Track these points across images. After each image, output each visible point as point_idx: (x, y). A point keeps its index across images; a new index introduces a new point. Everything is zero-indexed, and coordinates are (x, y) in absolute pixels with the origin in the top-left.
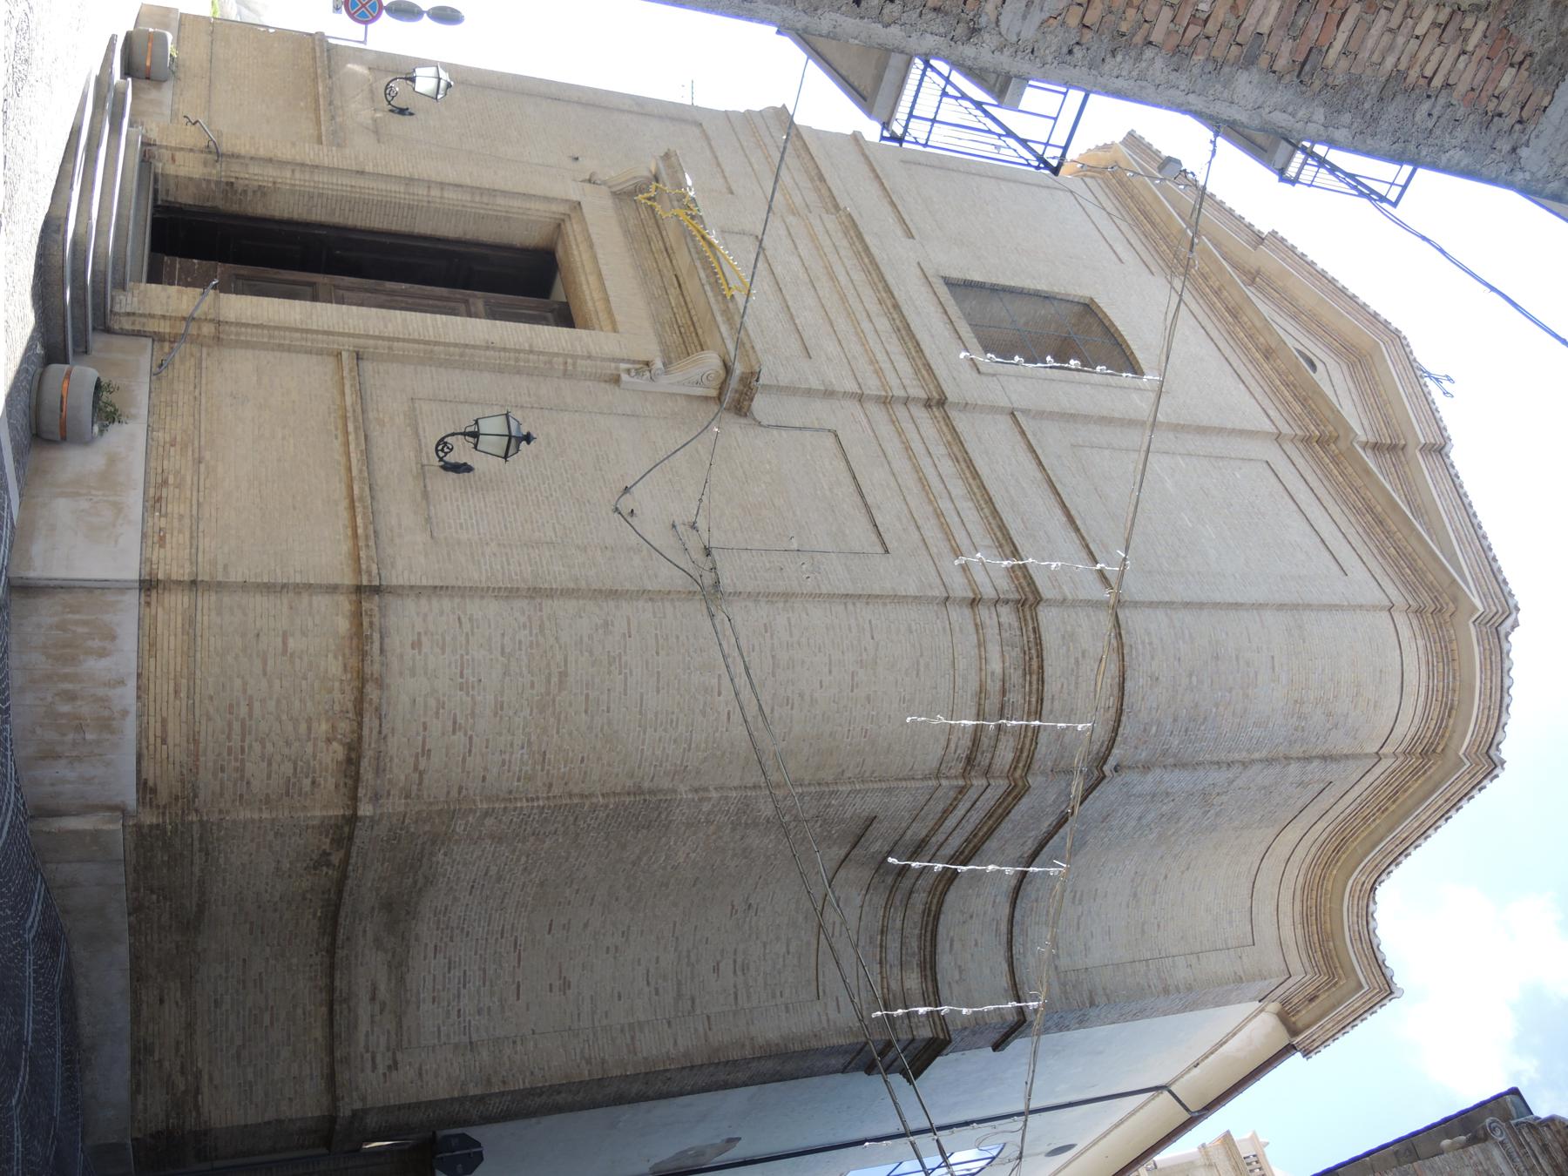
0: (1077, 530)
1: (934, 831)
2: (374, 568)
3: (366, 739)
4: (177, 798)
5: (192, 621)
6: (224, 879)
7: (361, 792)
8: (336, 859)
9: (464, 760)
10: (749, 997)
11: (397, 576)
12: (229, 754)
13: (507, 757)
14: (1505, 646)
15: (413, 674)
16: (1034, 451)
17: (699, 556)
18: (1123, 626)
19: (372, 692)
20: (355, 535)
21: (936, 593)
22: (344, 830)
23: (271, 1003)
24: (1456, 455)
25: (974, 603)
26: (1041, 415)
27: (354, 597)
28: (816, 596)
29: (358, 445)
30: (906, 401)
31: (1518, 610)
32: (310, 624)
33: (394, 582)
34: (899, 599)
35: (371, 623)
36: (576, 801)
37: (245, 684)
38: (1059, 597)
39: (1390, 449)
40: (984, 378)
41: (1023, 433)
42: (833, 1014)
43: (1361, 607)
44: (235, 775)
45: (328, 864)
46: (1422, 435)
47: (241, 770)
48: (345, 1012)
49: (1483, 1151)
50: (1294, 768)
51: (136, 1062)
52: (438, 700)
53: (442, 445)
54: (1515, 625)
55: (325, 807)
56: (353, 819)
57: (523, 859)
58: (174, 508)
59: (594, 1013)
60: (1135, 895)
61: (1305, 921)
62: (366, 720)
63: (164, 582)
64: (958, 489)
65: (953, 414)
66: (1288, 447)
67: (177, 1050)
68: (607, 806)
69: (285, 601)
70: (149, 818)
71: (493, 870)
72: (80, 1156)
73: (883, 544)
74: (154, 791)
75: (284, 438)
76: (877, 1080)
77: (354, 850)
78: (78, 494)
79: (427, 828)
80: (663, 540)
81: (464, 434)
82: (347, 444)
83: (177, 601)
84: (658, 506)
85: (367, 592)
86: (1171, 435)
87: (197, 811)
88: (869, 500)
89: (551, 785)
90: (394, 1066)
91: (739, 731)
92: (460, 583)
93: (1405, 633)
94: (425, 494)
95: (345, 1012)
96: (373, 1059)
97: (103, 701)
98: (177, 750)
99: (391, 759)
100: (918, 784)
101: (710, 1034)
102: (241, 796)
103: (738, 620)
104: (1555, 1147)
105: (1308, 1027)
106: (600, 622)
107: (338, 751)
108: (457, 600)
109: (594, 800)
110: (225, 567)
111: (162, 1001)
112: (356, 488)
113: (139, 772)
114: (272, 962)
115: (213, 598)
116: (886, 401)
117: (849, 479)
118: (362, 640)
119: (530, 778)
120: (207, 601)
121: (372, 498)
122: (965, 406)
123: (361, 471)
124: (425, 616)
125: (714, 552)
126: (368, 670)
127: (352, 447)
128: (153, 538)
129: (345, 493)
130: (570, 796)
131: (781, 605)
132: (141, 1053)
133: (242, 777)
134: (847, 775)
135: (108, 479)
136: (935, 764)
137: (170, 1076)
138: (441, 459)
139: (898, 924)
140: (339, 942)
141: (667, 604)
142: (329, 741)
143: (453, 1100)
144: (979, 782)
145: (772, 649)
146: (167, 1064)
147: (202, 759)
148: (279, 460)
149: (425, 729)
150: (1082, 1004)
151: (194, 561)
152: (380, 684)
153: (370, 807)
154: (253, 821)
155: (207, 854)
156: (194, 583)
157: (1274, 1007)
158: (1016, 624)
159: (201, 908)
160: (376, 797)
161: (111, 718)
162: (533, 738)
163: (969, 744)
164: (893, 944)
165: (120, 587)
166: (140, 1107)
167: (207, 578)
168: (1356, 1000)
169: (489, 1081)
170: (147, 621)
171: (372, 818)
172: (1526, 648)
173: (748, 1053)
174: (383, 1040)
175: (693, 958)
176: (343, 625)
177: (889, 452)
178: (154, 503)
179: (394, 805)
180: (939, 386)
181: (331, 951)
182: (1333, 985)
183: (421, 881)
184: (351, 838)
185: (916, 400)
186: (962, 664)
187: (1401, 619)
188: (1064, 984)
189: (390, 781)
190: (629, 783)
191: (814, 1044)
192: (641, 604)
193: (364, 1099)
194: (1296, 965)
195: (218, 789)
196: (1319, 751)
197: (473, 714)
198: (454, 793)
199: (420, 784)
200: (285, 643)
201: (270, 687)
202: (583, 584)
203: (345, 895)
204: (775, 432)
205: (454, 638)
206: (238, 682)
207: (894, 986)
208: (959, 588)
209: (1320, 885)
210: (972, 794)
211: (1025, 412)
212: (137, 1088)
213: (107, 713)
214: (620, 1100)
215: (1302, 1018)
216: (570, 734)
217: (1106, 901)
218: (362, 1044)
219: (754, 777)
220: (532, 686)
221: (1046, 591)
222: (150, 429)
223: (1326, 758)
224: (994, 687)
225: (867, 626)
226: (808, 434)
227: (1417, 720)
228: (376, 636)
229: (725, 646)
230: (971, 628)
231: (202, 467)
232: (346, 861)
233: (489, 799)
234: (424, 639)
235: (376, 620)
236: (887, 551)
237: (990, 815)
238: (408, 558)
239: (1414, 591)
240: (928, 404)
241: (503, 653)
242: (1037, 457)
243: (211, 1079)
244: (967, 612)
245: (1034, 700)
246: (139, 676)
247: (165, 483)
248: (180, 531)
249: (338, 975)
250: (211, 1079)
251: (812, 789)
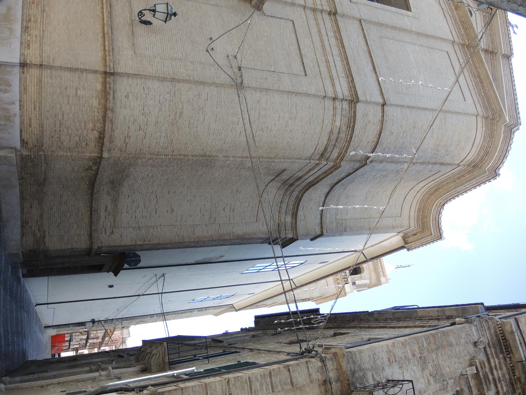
0: (376, 73)
1: (305, 175)
2: (112, 64)
3: (106, 131)
4: (35, 146)
5: (40, 81)
6: (53, 172)
7: (104, 149)
8: (94, 168)
9: (142, 140)
10: (234, 219)
11: (120, 69)
12: (55, 132)
13: (158, 140)
14: (512, 136)
15: (125, 108)
17: (236, 70)
18: (385, 113)
19: (109, 114)
20: (105, 49)
21: (322, 94)
22: (98, 160)
23: (70, 210)
24: (514, 60)
25: (334, 99)
26: (370, 22)
27: (103, 75)
28: (277, 91)
29: (107, 9)
30: (322, 11)
31: (520, 124)
32: (86, 85)
33: (119, 71)
34: (307, 95)
35: (110, 87)
36: (182, 157)
37: (61, 107)
38: (365, 100)
39: (491, 53)
40: (352, 4)
41: (363, 30)
42: (261, 227)
43: (467, 114)
44: (57, 140)
45: (91, 170)
46: (504, 50)
47: (60, 138)
48: (96, 214)
49: (470, 327)
50: (430, 166)
51: (23, 227)
52: (134, 118)
53: (141, 13)
54: (518, 129)
55: (91, 152)
56: (101, 158)
57: (161, 172)
58: (34, 32)
59: (181, 220)
60: (366, 198)
61: (419, 211)
62: (107, 124)
63: (30, 64)
64: (336, 52)
65: (338, 18)
66: (456, 47)
67: (37, 223)
68: (193, 160)
69: (77, 75)
70: (25, 153)
71: (150, 175)
72: (3, 257)
73: (305, 71)
74: (27, 143)
75: (77, 3)
76: (271, 246)
77: (101, 167)
79: (128, 161)
80: (221, 60)
81: (150, 10)
82: (103, 8)
83: (35, 72)
84: (223, 48)
85: (108, 75)
86: (416, 37)
87: (43, 150)
88: (302, 52)
89: (173, 151)
90: (112, 233)
91: (243, 138)
92: (144, 74)
93: (480, 125)
94: (133, 33)
95: (96, 214)
96: (105, 230)
97: (6, 110)
98: (35, 129)
99: (116, 138)
100: (303, 161)
101: (220, 230)
102: (60, 147)
103: (248, 98)
104: (492, 327)
105: (411, 243)
106: (197, 94)
107: (96, 134)
108: (143, 80)
109: (189, 157)
110: (54, 59)
111: (31, 207)
112: (105, 28)
113: (21, 136)
114: (70, 197)
115: (49, 71)
116: (314, 10)
117: (296, 43)
118: (106, 93)
119: (166, 148)
120: (46, 73)
121: (112, 33)
122: (343, 16)
123: (108, 21)
124: (131, 85)
125: (242, 69)
126: (108, 106)
127: (105, 10)
128: (25, 45)
129: (101, 30)
130: (180, 155)
131: (264, 93)
132: (24, 224)
133: (60, 141)
134: (279, 156)
136: (310, 155)
137: (34, 231)
138: (140, 19)
139: (287, 201)
140: (95, 192)
141: (223, 89)
142: (93, 130)
143: (132, 245)
144: (324, 163)
145: (259, 110)
146: (33, 227)
147: (45, 133)
148: (75, 13)
149: (129, 128)
150: (343, 229)
151: (41, 56)
152: (112, 111)
153: (107, 154)
154: (64, 156)
155: (47, 164)
156: (41, 65)
157: (401, 234)
158: (348, 109)
159: (45, 180)
160: (109, 150)
161: (10, 117)
162: (169, 135)
163: (323, 150)
164: (284, 206)
165: (13, 65)
166: (24, 241)
167: (46, 64)
168: (429, 238)
169: (144, 240)
170: (23, 80)
171: (108, 158)
172: (519, 137)
173: (231, 237)
174: (109, 224)
175: (216, 206)
176: (99, 87)
177: (312, 32)
178: (25, 29)
179: (116, 154)
180: (335, 6)
181: (92, 194)
182: (424, 230)
183: (124, 176)
184: (100, 163)
185: (326, 11)
186: (326, 122)
187: (480, 120)
188: (337, 224)
189: (115, 145)
190: (202, 153)
191: (253, 236)
192: (213, 88)
193: (102, 243)
194: (412, 225)
195: (51, 144)
196: (440, 162)
197: (147, 125)
198: (138, 151)
199: (126, 147)
200: (76, 92)
201: (71, 108)
202: (192, 78)
203: (97, 179)
204: (270, 19)
205: (141, 95)
206: (58, 106)
207: (282, 220)
208: (330, 93)
209: (427, 200)
210: (321, 166)
211: (365, 21)
212: (23, 235)
213: (8, 114)
214: (187, 247)
215: (410, 240)
216: (182, 134)
217: (355, 201)
218: (102, 225)
219: (246, 154)
220: (170, 116)
221: (361, 98)
223: (441, 164)
224: (336, 131)
225: (295, 104)
226: (283, 21)
227: (475, 155)
228: (112, 92)
229: (242, 107)
230: (332, 108)
231: (45, 13)
232: (98, 169)
233: (151, 154)
234: (130, 95)
235: (112, 86)
236: (306, 75)
237: (325, 172)
238: (125, 62)
239: (486, 110)
240: (329, 13)
241: (159, 103)
242: (366, 41)
243: (49, 233)
244: (331, 102)
245: (349, 137)
246: (20, 101)
248: (36, 43)
249: (94, 202)
250: (49, 233)
251: (266, 160)
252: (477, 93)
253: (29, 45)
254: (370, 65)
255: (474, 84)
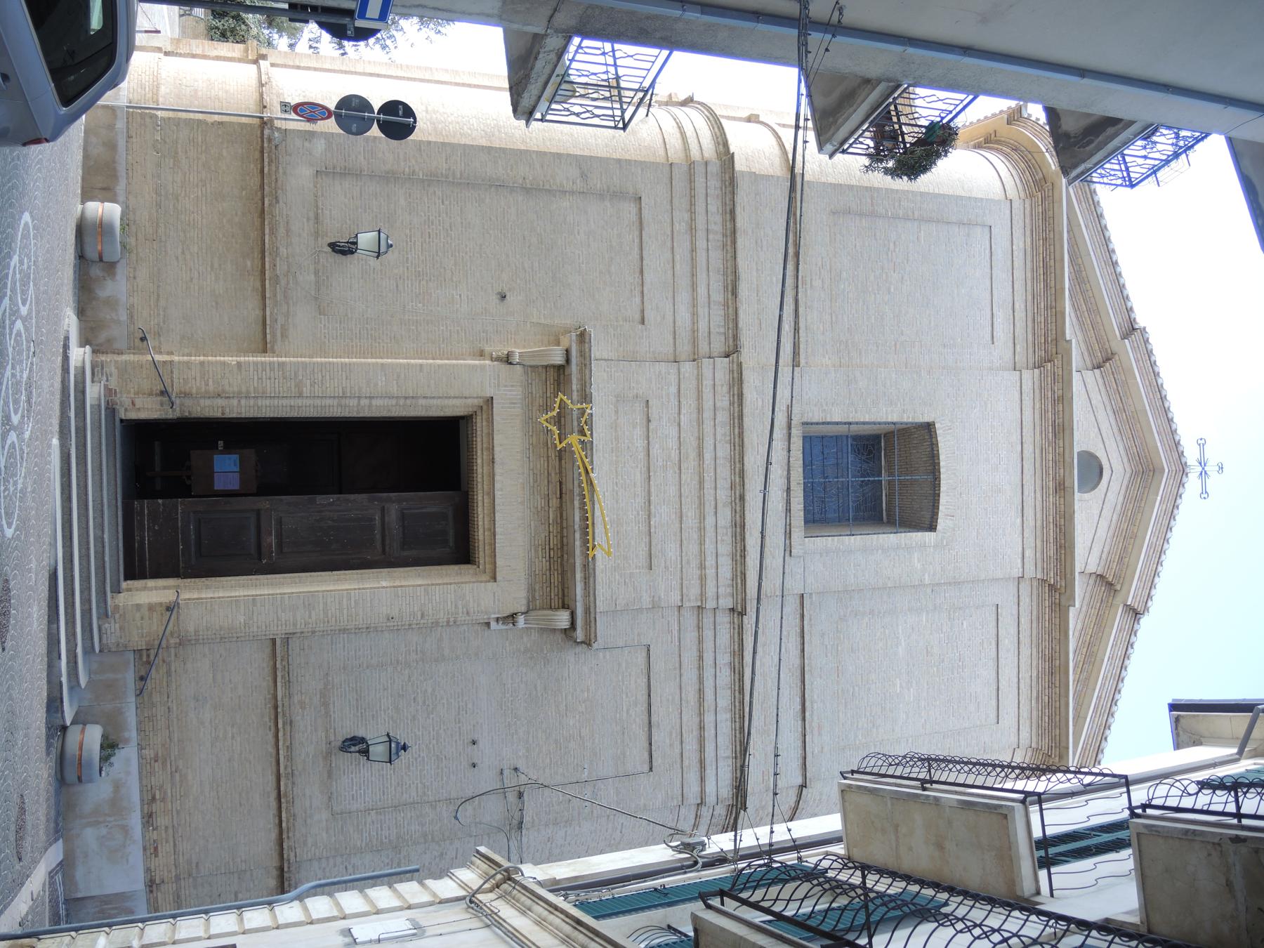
16: (803, 637)
24: (1145, 621)
41: (802, 616)
58: (161, 821)
75: (233, 737)
78: (98, 823)
135: (116, 804)
178: (148, 818)
222: (141, 747)
247: (154, 798)
252: (1034, 694)
253: (156, 849)
254: (798, 700)
255: (1034, 674)
